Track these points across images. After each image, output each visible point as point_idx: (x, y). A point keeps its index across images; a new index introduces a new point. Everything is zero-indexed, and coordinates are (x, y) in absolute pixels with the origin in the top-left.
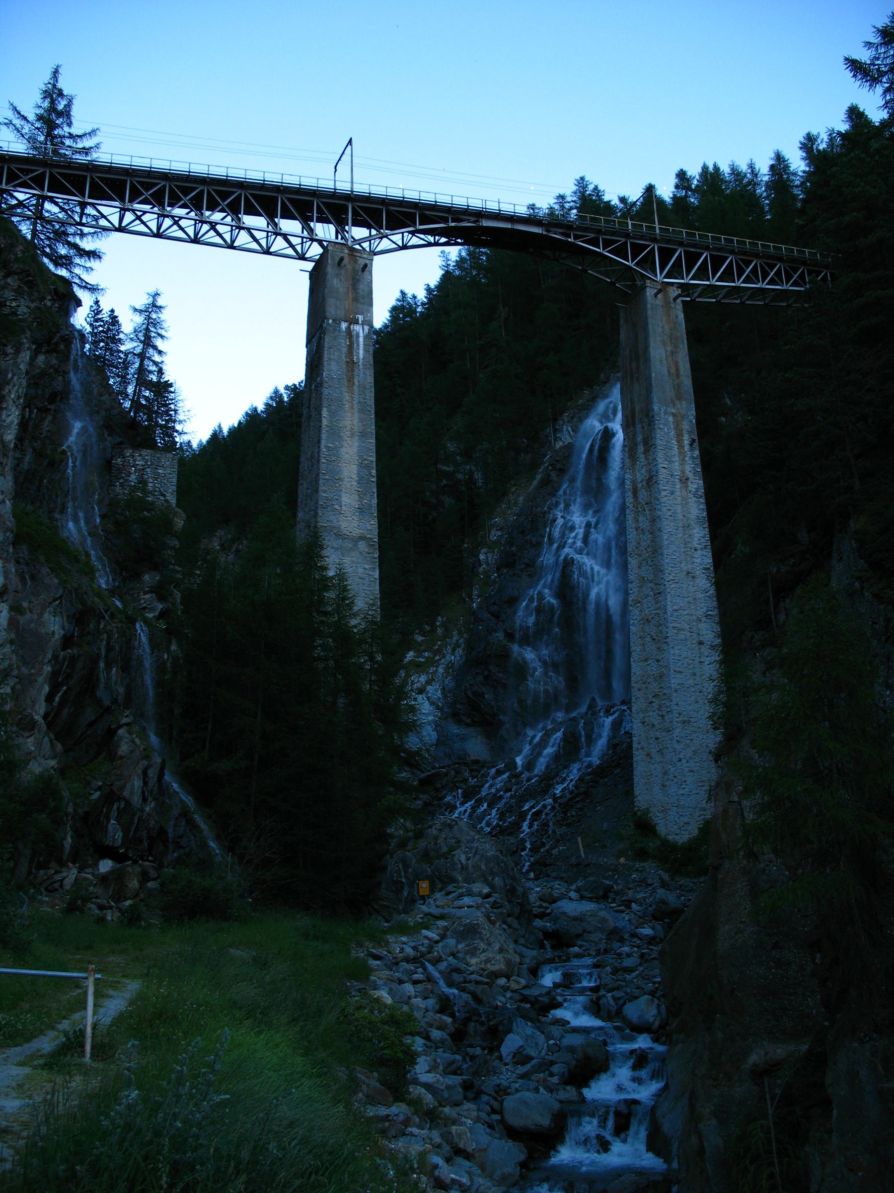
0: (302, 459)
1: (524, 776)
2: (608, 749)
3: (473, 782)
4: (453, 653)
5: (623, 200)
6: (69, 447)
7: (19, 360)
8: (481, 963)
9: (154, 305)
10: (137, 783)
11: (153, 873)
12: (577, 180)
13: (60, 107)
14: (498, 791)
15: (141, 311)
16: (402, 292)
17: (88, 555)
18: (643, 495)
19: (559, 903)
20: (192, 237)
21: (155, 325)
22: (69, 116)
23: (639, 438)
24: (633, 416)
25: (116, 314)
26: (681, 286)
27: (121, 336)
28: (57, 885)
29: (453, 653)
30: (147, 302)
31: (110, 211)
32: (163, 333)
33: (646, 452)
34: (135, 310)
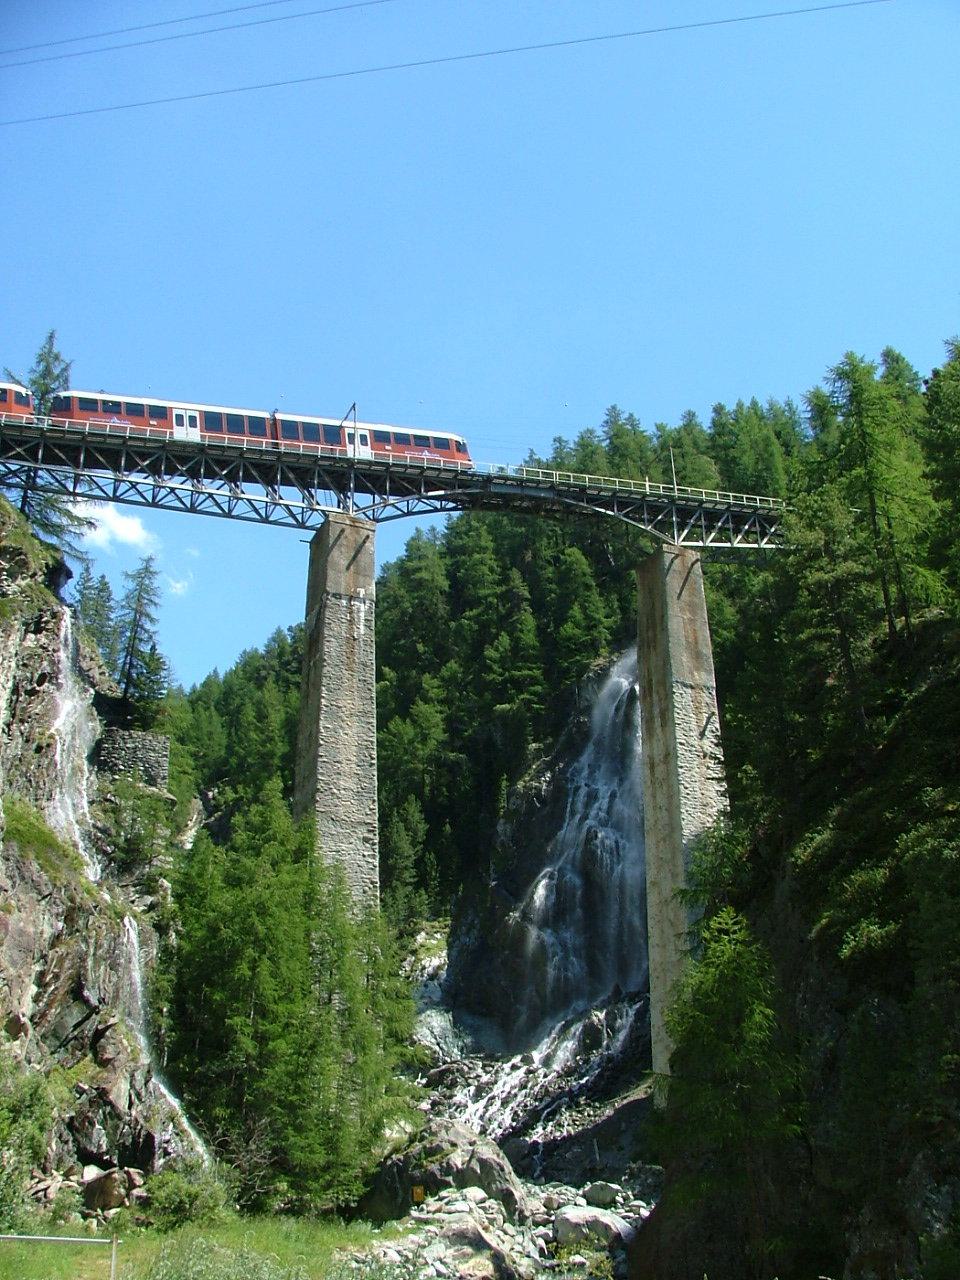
0: (301, 737)
1: (541, 1072)
2: (631, 1041)
3: (485, 1078)
4: (467, 934)
5: (660, 427)
6: (57, 730)
7: (9, 643)
8: (469, 1269)
9: (146, 569)
10: (124, 1086)
11: (139, 1180)
12: (608, 410)
13: (56, 371)
14: (512, 1088)
15: (133, 577)
16: (417, 529)
17: (75, 845)
18: (660, 770)
19: (564, 1209)
20: (189, 506)
21: (147, 593)
22: (66, 381)
23: (656, 711)
24: (650, 688)
25: (106, 580)
26: (702, 549)
27: (112, 603)
28: (41, 1194)
29: (467, 934)
30: (141, 567)
31: (105, 476)
32: (157, 600)
33: (663, 725)
34: (127, 575)
